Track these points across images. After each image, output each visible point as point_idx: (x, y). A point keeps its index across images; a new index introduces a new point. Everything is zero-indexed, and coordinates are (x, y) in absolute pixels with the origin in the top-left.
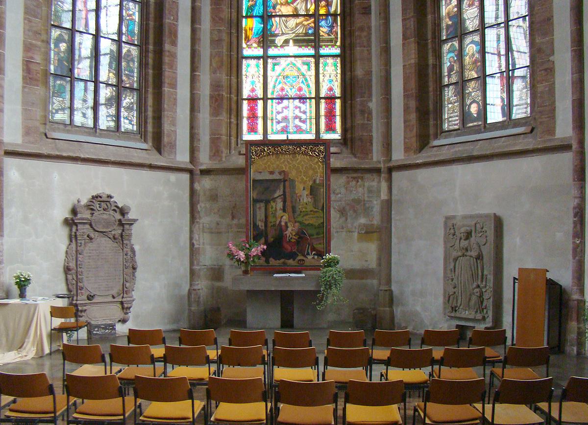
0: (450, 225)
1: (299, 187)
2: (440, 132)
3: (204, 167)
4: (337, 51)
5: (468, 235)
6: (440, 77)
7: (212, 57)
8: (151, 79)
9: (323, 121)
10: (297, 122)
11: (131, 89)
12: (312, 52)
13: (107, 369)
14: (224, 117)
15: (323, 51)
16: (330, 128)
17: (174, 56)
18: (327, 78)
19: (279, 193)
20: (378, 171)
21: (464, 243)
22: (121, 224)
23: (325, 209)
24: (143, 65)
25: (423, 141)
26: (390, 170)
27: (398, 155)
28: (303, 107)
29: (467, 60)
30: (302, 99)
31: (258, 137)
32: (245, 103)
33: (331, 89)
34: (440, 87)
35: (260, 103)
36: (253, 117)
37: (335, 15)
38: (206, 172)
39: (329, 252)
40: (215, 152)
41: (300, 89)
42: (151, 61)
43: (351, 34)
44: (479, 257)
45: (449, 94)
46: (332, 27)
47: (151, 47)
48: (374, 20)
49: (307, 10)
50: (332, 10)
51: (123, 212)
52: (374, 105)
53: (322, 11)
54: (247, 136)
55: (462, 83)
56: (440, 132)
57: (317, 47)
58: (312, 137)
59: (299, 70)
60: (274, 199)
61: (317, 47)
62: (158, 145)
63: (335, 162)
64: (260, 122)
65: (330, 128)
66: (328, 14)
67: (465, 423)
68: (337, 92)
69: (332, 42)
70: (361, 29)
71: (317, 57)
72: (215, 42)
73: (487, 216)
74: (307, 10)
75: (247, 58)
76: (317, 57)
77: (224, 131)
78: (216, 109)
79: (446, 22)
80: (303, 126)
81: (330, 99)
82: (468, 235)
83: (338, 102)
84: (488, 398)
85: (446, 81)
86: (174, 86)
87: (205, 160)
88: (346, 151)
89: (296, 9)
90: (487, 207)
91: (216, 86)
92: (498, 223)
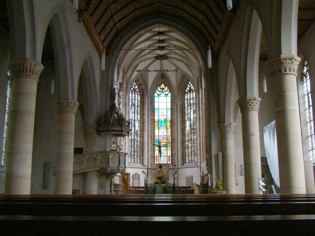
0: (186, 178)
1: (164, 171)
2: (186, 163)
3: (149, 168)
4: (170, 149)
5: (188, 179)
6: (186, 154)
7: (151, 150)
8: (141, 154)
9: (168, 160)
10: (164, 160)
11: (139, 156)
12: (166, 149)
13: (242, 179)
14: (152, 160)
15: (168, 148)
16: (169, 161)
17: (145, 150)
18: (169, 153)
19: (161, 172)
20: (176, 169)
21: (188, 180)
22: (139, 177)
23: (168, 175)
24: (140, 152)
25: (183, 164)
26: (178, 169)
27: (180, 166)
28: (165, 158)
29: (189, 152)
30: (165, 156)
31: (158, 163)
32: (155, 157)
33: (169, 155)
34: (186, 156)
35: (158, 157)
36: (157, 159)
37: (170, 142)
38: (150, 169)
39: (169, 181)
40: (151, 166)
41: (164, 155)
42: (141, 151)
43: (172, 146)
44: (190, 182)
45: (187, 157)
46: (169, 145)
47: (142, 149)
48: (176, 144)
49: (165, 142)
50: (170, 142)
51: (139, 175)
52: (176, 158)
53: (168, 142)
54: (156, 163)
55: (189, 156)
56: (186, 163)
57: (167, 148)
58: (166, 163)
59: (164, 152)
60: (161, 173)
61: (167, 148)
62: (143, 164)
63: (170, 167)
64: (158, 160)
65: (169, 161)
66: (169, 142)
67: (188, 204)
68: (170, 155)
69: (170, 147)
70: (174, 146)
71: (167, 150)
72: (151, 148)
73: (190, 176)
74: (165, 142)
75: (156, 150)
76: (167, 150)
77: (152, 162)
78: (151, 159)
79: (187, 145)
80: (165, 161)
81: (169, 157)
82: (188, 179)
83: (170, 157)
84: (126, 85)
85: (187, 155)
86: (145, 155)
87: (150, 167)
88: (172, 165)
89: (164, 141)
90: (191, 174)
91: (151, 155)
92: (192, 177)
